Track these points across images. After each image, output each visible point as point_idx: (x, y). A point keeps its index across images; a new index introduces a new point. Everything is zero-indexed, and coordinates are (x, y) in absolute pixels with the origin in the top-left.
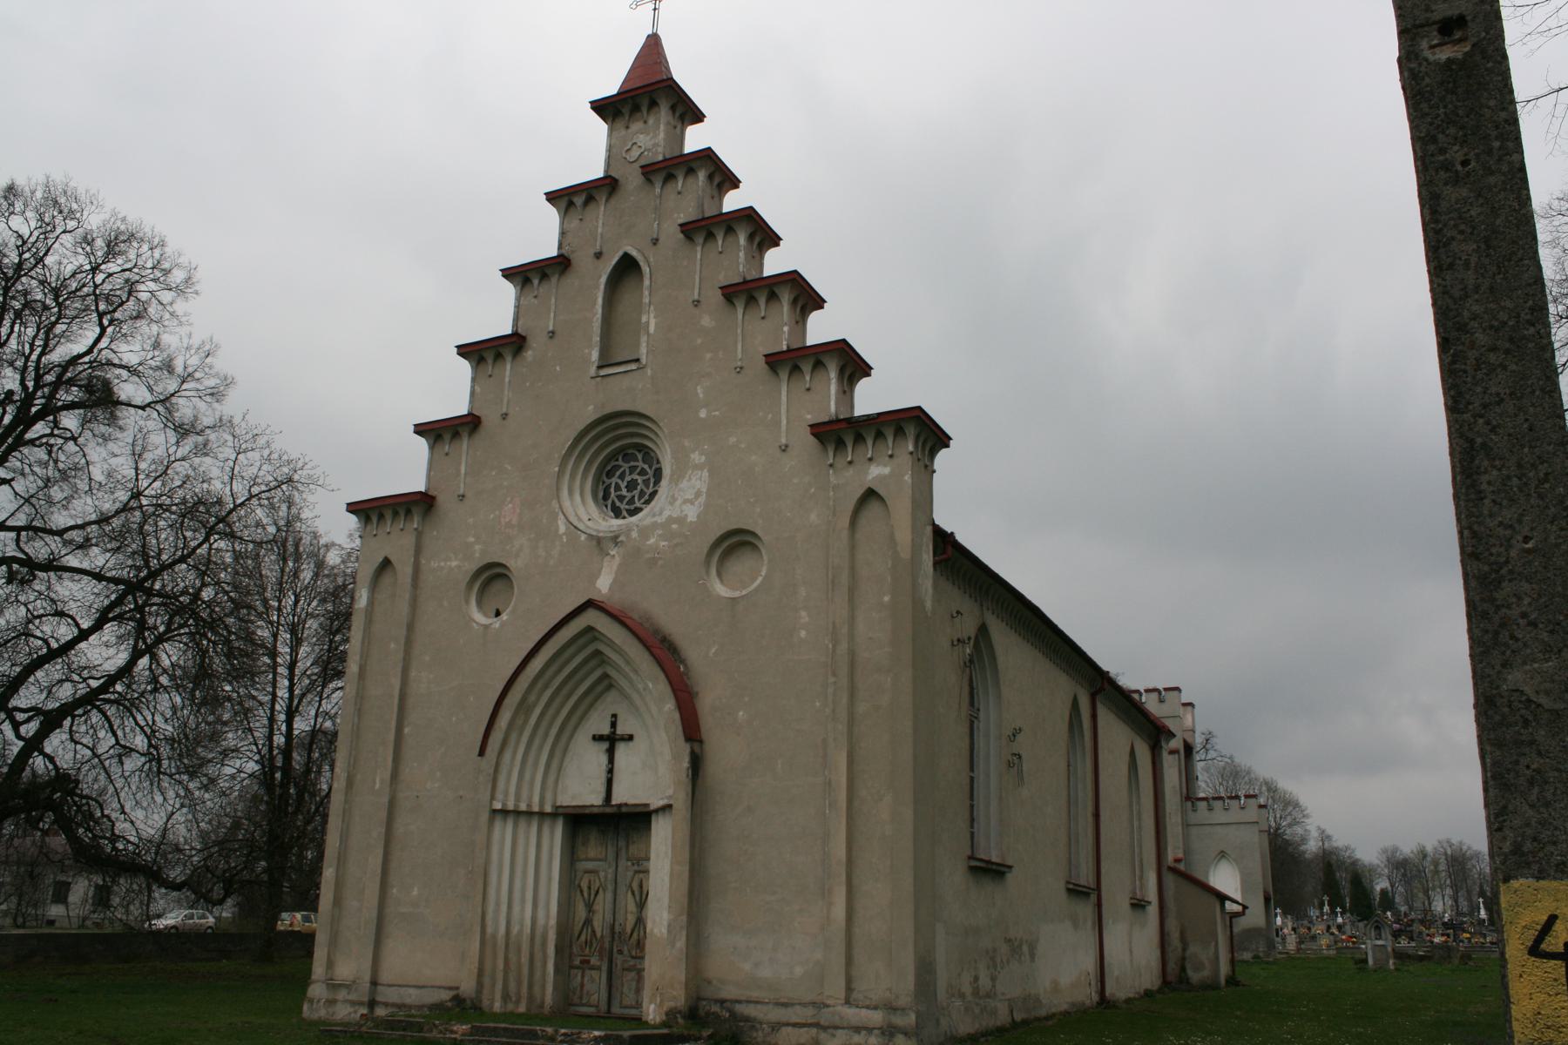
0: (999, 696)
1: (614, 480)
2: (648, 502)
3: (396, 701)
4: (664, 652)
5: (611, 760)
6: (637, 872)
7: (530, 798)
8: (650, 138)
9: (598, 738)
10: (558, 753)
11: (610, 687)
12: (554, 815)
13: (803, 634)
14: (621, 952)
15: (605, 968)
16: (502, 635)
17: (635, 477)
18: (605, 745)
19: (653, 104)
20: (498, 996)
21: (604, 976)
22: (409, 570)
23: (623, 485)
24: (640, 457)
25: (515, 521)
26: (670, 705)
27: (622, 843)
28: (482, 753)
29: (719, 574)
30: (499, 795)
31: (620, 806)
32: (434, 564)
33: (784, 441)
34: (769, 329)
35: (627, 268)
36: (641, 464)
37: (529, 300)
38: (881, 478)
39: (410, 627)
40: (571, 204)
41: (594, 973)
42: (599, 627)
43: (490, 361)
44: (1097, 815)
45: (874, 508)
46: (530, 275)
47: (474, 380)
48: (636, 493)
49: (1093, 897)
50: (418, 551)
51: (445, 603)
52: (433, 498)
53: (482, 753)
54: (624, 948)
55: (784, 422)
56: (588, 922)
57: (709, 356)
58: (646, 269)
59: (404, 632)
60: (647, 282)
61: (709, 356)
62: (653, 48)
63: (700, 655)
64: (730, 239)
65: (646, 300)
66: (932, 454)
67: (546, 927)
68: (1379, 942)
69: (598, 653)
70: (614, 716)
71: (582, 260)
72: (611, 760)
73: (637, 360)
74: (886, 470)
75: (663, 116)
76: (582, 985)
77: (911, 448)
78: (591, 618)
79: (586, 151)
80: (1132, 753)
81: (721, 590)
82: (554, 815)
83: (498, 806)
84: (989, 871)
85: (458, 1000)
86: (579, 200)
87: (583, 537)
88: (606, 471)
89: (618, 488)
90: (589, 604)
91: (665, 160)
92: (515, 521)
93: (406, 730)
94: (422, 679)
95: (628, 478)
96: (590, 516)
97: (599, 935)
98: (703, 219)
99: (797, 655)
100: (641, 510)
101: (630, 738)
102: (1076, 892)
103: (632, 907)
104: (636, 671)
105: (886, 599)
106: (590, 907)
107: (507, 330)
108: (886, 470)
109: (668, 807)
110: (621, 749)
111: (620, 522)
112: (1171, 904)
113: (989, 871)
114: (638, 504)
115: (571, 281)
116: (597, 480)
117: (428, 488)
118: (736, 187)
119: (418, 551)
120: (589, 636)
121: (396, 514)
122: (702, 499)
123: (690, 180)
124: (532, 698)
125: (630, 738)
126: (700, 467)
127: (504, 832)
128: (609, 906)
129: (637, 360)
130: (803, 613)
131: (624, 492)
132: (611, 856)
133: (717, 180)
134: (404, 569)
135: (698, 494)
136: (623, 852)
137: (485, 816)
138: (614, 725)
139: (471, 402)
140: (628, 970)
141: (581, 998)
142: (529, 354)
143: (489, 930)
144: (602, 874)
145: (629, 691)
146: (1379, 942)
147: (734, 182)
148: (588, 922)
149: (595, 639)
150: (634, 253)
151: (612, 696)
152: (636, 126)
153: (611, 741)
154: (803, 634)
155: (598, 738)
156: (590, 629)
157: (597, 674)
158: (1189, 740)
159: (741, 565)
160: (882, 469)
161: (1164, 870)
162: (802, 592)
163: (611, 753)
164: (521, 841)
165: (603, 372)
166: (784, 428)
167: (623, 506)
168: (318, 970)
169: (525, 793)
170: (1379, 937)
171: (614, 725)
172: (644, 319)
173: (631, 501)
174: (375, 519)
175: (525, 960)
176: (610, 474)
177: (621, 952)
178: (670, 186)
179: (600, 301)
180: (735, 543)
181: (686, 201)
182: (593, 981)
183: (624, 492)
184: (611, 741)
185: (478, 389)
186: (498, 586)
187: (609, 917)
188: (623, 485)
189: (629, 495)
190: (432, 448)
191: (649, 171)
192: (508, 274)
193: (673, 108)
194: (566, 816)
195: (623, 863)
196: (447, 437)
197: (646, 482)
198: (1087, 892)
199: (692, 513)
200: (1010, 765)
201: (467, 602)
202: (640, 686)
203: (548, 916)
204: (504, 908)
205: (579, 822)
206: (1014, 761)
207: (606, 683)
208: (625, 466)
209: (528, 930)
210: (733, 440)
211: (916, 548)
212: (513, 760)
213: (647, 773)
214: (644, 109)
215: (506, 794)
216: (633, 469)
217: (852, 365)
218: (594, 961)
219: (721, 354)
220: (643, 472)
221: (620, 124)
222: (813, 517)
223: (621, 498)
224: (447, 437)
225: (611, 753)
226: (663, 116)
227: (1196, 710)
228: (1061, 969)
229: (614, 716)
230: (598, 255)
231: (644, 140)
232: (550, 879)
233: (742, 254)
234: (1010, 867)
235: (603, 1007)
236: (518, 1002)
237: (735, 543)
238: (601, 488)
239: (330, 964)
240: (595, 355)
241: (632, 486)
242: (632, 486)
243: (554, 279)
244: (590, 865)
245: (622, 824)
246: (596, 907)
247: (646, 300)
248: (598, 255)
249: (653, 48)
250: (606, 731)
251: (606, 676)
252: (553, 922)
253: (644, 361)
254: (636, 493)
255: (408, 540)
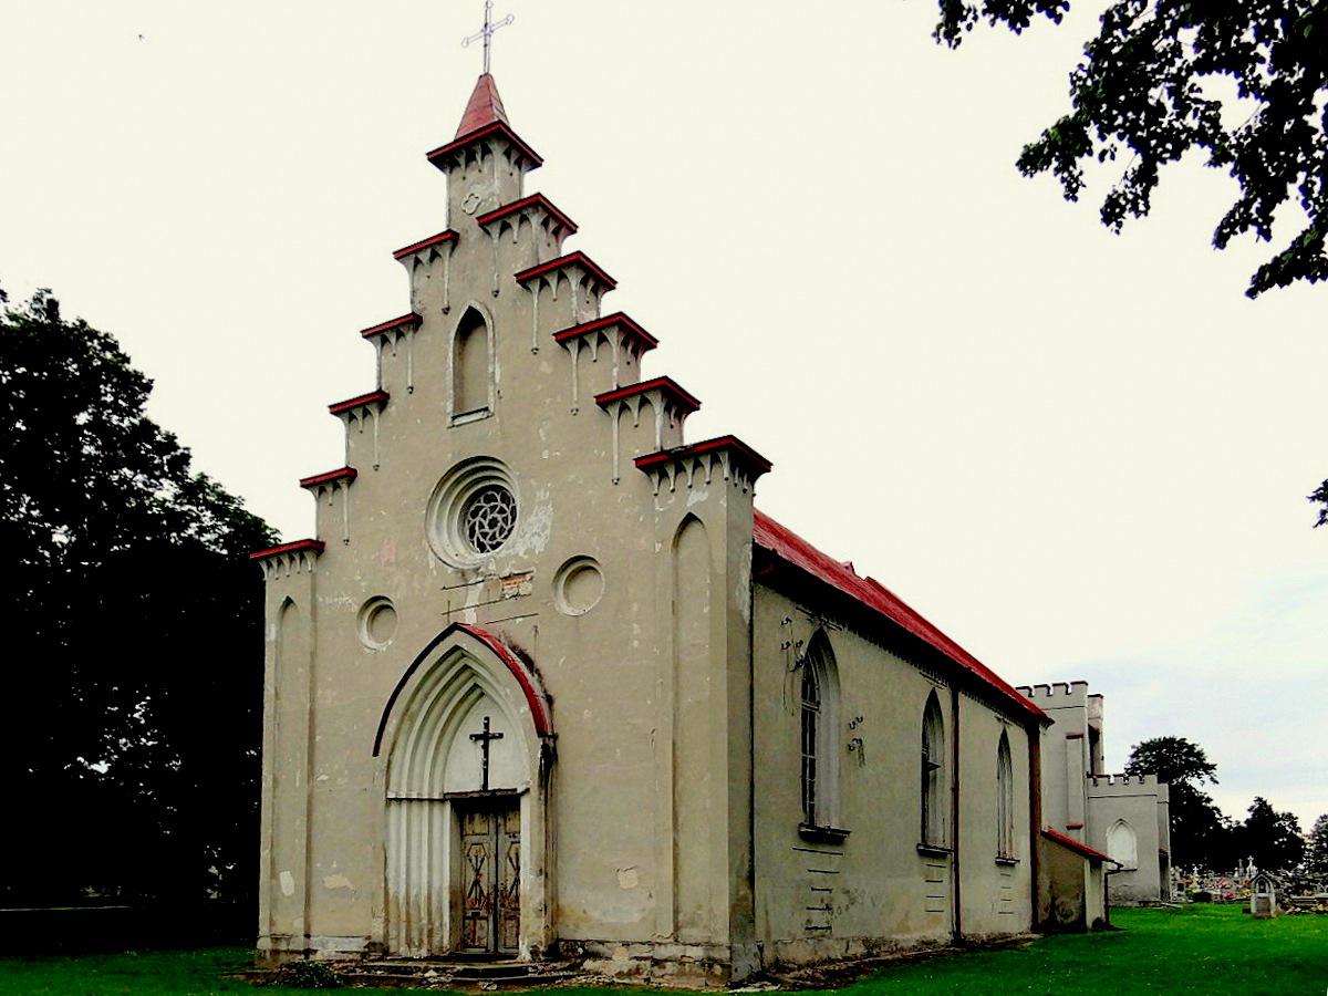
0: (839, 692)
1: (478, 519)
2: (506, 537)
3: (307, 716)
4: (521, 664)
5: (486, 755)
6: (512, 843)
7: (421, 788)
8: (492, 182)
9: (476, 737)
10: (443, 750)
11: (482, 694)
12: (442, 801)
13: (636, 643)
14: (503, 905)
15: (491, 919)
16: (385, 653)
17: (495, 515)
18: (481, 743)
19: (486, 151)
20: (403, 941)
21: (491, 926)
22: (308, 607)
23: (486, 523)
24: (499, 498)
25: (393, 560)
26: (525, 708)
27: (500, 821)
28: (376, 753)
29: (566, 596)
30: (393, 787)
31: (495, 791)
32: (329, 600)
33: (616, 476)
34: (607, 368)
35: (472, 323)
36: (499, 503)
37: (388, 358)
38: (700, 503)
39: (313, 655)
40: (418, 262)
41: (483, 922)
42: (464, 646)
43: (360, 418)
44: (955, 790)
45: (694, 529)
46: (387, 334)
47: (348, 436)
48: (497, 529)
49: (950, 857)
50: (314, 590)
51: (341, 633)
52: (323, 544)
53: (376, 753)
54: (503, 905)
55: (616, 457)
56: (477, 883)
57: (548, 401)
58: (489, 322)
59: (309, 659)
60: (490, 334)
61: (548, 401)
62: (486, 84)
63: (554, 668)
64: (563, 285)
65: (491, 352)
66: (752, 480)
67: (441, 888)
68: (1262, 895)
69: (466, 667)
70: (487, 719)
71: (432, 316)
72: (486, 755)
73: (486, 409)
74: (704, 496)
75: (498, 162)
76: (474, 932)
77: (726, 475)
78: (457, 638)
79: (427, 204)
80: (1004, 738)
81: (566, 609)
82: (442, 801)
83: (391, 795)
84: (819, 837)
85: (372, 946)
86: (425, 256)
87: (450, 570)
88: (470, 511)
89: (481, 526)
90: (455, 627)
91: (501, 208)
92: (393, 560)
93: (318, 738)
94: (326, 697)
95: (489, 517)
96: (454, 547)
97: (485, 893)
98: (539, 266)
99: (646, 667)
100: (501, 543)
101: (501, 736)
102: (926, 852)
103: (510, 870)
104: (498, 682)
105: (706, 610)
106: (477, 871)
107: (373, 389)
108: (704, 496)
109: (527, 790)
110: (493, 744)
111: (484, 555)
112: (1042, 858)
113: (819, 837)
114: (499, 540)
115: (424, 335)
116: (463, 519)
117: (318, 537)
118: (574, 232)
119: (314, 590)
120: (457, 654)
121: (292, 559)
122: (548, 532)
123: (525, 227)
124: (414, 707)
125: (501, 736)
126: (546, 503)
127: (398, 814)
128: (493, 870)
129: (486, 409)
130: (635, 625)
131: (487, 529)
132: (492, 831)
133: (552, 226)
134: (304, 604)
135: (544, 528)
136: (502, 829)
137: (383, 803)
138: (487, 726)
139: (347, 456)
140: (510, 918)
141: (473, 941)
142: (392, 409)
143: (391, 892)
144: (486, 846)
145: (497, 698)
146: (1262, 895)
147: (571, 228)
148: (477, 883)
149: (464, 656)
150: (478, 307)
151: (484, 701)
152: (472, 175)
153: (485, 738)
154: (636, 643)
155: (476, 737)
156: (456, 648)
157: (470, 684)
158: (1094, 726)
159: (586, 584)
160: (705, 492)
161: (1038, 837)
162: (635, 607)
163: (486, 748)
164: (415, 823)
165: (457, 422)
166: (616, 463)
167: (486, 542)
168: (264, 929)
169: (416, 783)
170: (1263, 891)
171: (487, 726)
172: (491, 370)
173: (493, 537)
174: (297, 558)
175: (424, 914)
176: (474, 515)
177: (503, 905)
178: (506, 235)
179: (451, 355)
180: (578, 567)
181: (528, 245)
182: (482, 928)
183: (487, 529)
184: (485, 738)
185: (352, 445)
186: (384, 616)
187: (493, 879)
188: (486, 523)
189: (491, 532)
190: (318, 500)
191: (485, 222)
192: (368, 334)
193: (507, 154)
194: (452, 800)
195: (502, 836)
196: (330, 489)
197: (505, 520)
198: (938, 853)
199: (539, 545)
200: (850, 748)
201: (359, 628)
202: (503, 694)
203: (442, 879)
204: (403, 869)
205: (467, 807)
206: (855, 748)
207: (478, 692)
208: (487, 506)
209: (425, 892)
210: (572, 477)
211: (731, 566)
212: (402, 759)
213: (513, 767)
214: (478, 157)
215: (399, 785)
216: (493, 509)
217: (680, 402)
218: (483, 913)
219: (559, 399)
220: (502, 511)
221: (458, 172)
222: (642, 541)
223: (484, 535)
224: (330, 489)
225: (486, 748)
226: (498, 162)
227: (1104, 700)
228: (912, 912)
229: (487, 719)
230: (446, 311)
231: (479, 190)
232: (442, 851)
233: (574, 299)
234: (848, 833)
235: (491, 948)
236: (420, 947)
237: (578, 567)
238: (467, 526)
239: (272, 923)
240: (450, 407)
241: (493, 524)
242: (493, 524)
243: (409, 335)
244: (475, 839)
245: (493, 806)
246: (481, 871)
247: (491, 352)
248: (446, 311)
249: (486, 84)
250: (481, 731)
251: (476, 686)
252: (447, 884)
253: (492, 410)
254: (497, 529)
255: (305, 581)
